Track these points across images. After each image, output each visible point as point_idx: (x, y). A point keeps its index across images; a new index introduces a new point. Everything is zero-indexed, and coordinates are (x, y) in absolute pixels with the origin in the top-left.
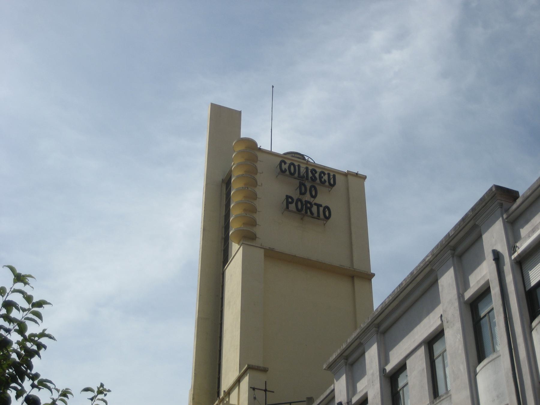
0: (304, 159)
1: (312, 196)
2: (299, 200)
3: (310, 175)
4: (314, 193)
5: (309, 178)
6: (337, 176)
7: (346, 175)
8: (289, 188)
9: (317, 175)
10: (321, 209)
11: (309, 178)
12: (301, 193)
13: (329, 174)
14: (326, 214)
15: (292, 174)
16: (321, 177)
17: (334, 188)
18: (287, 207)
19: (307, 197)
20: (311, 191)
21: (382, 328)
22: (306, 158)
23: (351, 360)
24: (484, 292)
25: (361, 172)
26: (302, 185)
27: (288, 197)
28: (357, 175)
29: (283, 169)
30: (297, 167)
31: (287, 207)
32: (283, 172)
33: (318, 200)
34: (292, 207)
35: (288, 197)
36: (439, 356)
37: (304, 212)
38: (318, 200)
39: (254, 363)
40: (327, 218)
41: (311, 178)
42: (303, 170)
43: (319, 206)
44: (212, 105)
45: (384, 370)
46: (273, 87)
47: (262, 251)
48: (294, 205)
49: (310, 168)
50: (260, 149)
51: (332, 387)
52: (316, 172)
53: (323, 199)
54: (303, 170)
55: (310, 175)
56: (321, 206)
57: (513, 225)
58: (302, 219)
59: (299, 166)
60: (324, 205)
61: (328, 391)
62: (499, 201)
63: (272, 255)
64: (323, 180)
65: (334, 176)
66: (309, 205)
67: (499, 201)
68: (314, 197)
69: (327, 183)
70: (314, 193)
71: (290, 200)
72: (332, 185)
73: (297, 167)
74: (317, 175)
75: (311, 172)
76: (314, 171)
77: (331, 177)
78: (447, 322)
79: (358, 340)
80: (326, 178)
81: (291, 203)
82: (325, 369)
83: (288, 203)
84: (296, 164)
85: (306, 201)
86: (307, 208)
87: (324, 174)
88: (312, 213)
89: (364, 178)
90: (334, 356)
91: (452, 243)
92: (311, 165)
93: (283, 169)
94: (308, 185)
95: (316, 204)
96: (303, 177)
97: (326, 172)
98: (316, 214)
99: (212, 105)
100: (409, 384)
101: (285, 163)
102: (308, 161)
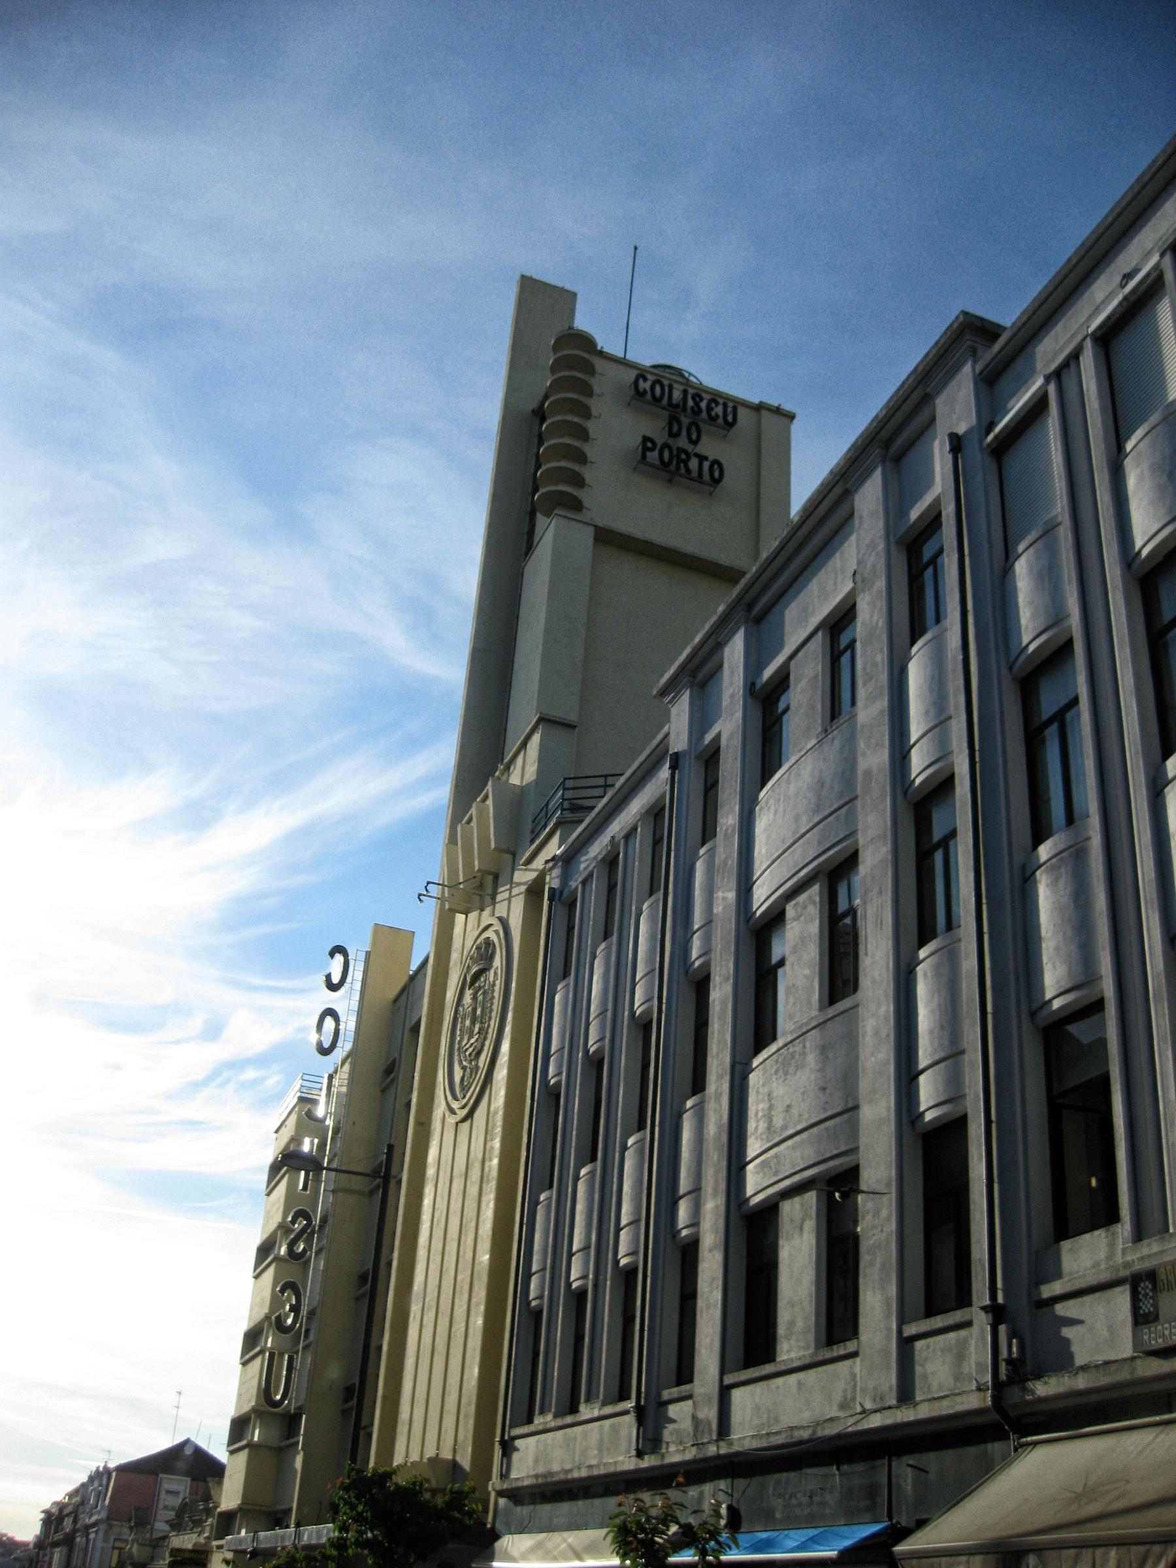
0: (682, 375)
1: (691, 441)
2: (666, 446)
3: (690, 403)
4: (694, 437)
5: (689, 410)
6: (741, 412)
7: (759, 408)
8: (653, 426)
9: (703, 405)
10: (706, 465)
11: (689, 410)
12: (672, 435)
13: (725, 406)
14: (714, 476)
15: (657, 400)
16: (709, 409)
17: (733, 430)
18: (644, 457)
19: (682, 442)
20: (689, 428)
21: (757, 609)
22: (687, 375)
23: (700, 676)
24: (932, 522)
25: (787, 406)
26: (673, 419)
27: (646, 439)
28: (777, 411)
29: (641, 389)
30: (667, 389)
31: (644, 457)
32: (640, 394)
33: (701, 449)
34: (653, 456)
35: (646, 439)
36: (845, 651)
37: (673, 468)
38: (701, 449)
39: (556, 713)
40: (716, 481)
41: (692, 408)
42: (677, 395)
43: (702, 458)
44: (523, 277)
45: (753, 684)
46: (636, 248)
47: (590, 531)
48: (656, 453)
49: (691, 391)
50: (601, 354)
51: (666, 729)
52: (701, 399)
53: (710, 447)
54: (677, 395)
55: (690, 403)
56: (706, 458)
57: (992, 382)
58: (670, 481)
59: (671, 387)
60: (711, 458)
61: (660, 737)
62: (969, 343)
63: (605, 538)
64: (713, 413)
65: (735, 409)
66: (683, 456)
67: (969, 343)
68: (695, 443)
69: (721, 421)
70: (694, 437)
71: (649, 445)
72: (730, 425)
73: (667, 389)
74: (703, 405)
75: (693, 398)
76: (697, 397)
77: (729, 410)
78: (863, 581)
79: (713, 637)
80: (719, 410)
81: (652, 450)
82: (655, 697)
83: (645, 449)
84: (666, 383)
85: (678, 449)
86: (680, 461)
87: (717, 404)
88: (688, 471)
89: (791, 417)
90: (671, 671)
91: (884, 434)
92: (692, 387)
93: (641, 389)
94: (685, 421)
95: (697, 455)
96: (677, 406)
97: (721, 401)
98: (695, 474)
99: (523, 277)
100: (792, 706)
101: (645, 380)
102: (688, 380)
